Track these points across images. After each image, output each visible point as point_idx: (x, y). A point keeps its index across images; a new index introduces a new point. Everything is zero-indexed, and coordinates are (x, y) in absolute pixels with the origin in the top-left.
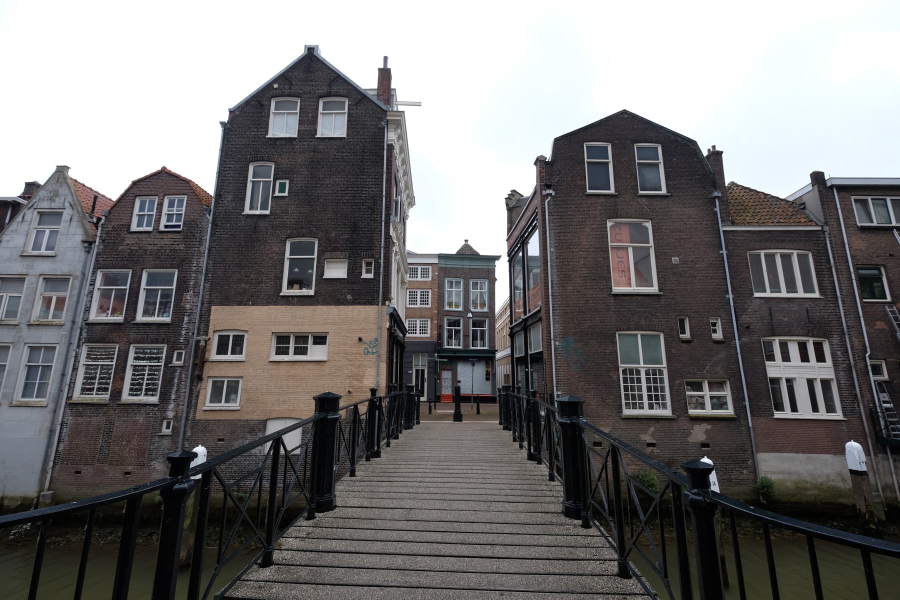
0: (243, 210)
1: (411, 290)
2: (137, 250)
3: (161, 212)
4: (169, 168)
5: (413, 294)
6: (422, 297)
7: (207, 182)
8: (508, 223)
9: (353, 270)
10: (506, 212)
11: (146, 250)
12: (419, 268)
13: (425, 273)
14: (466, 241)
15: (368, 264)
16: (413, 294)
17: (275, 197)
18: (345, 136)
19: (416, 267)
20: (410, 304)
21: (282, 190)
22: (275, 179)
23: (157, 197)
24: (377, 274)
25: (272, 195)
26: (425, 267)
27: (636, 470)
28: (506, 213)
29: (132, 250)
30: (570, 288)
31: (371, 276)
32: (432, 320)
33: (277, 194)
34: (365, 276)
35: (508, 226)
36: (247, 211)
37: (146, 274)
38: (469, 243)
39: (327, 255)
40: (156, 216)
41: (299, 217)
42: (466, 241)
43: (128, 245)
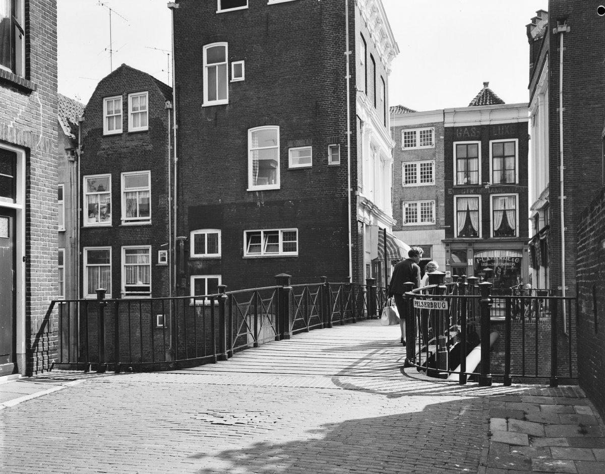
0: (202, 102)
1: (408, 163)
2: (112, 154)
3: (127, 112)
4: (127, 64)
5: (411, 168)
6: (414, 172)
7: (165, 73)
8: (530, 63)
9: (319, 156)
10: (529, 45)
11: (120, 154)
12: (418, 131)
13: (426, 137)
14: (486, 84)
15: (334, 150)
16: (411, 168)
17: (233, 83)
18: (279, 188)
19: (413, 130)
20: (406, 182)
21: (239, 72)
22: (230, 62)
23: (121, 96)
24: (344, 160)
25: (229, 82)
26: (426, 129)
27: (498, 314)
28: (527, 47)
29: (108, 155)
30: (587, 158)
31: (338, 163)
32: (437, 202)
33: (234, 79)
34: (331, 162)
35: (530, 66)
36: (206, 103)
37: (282, 234)
38: (490, 87)
39: (290, 143)
40: (123, 117)
41: (258, 104)
42: (486, 84)
43: (104, 149)
